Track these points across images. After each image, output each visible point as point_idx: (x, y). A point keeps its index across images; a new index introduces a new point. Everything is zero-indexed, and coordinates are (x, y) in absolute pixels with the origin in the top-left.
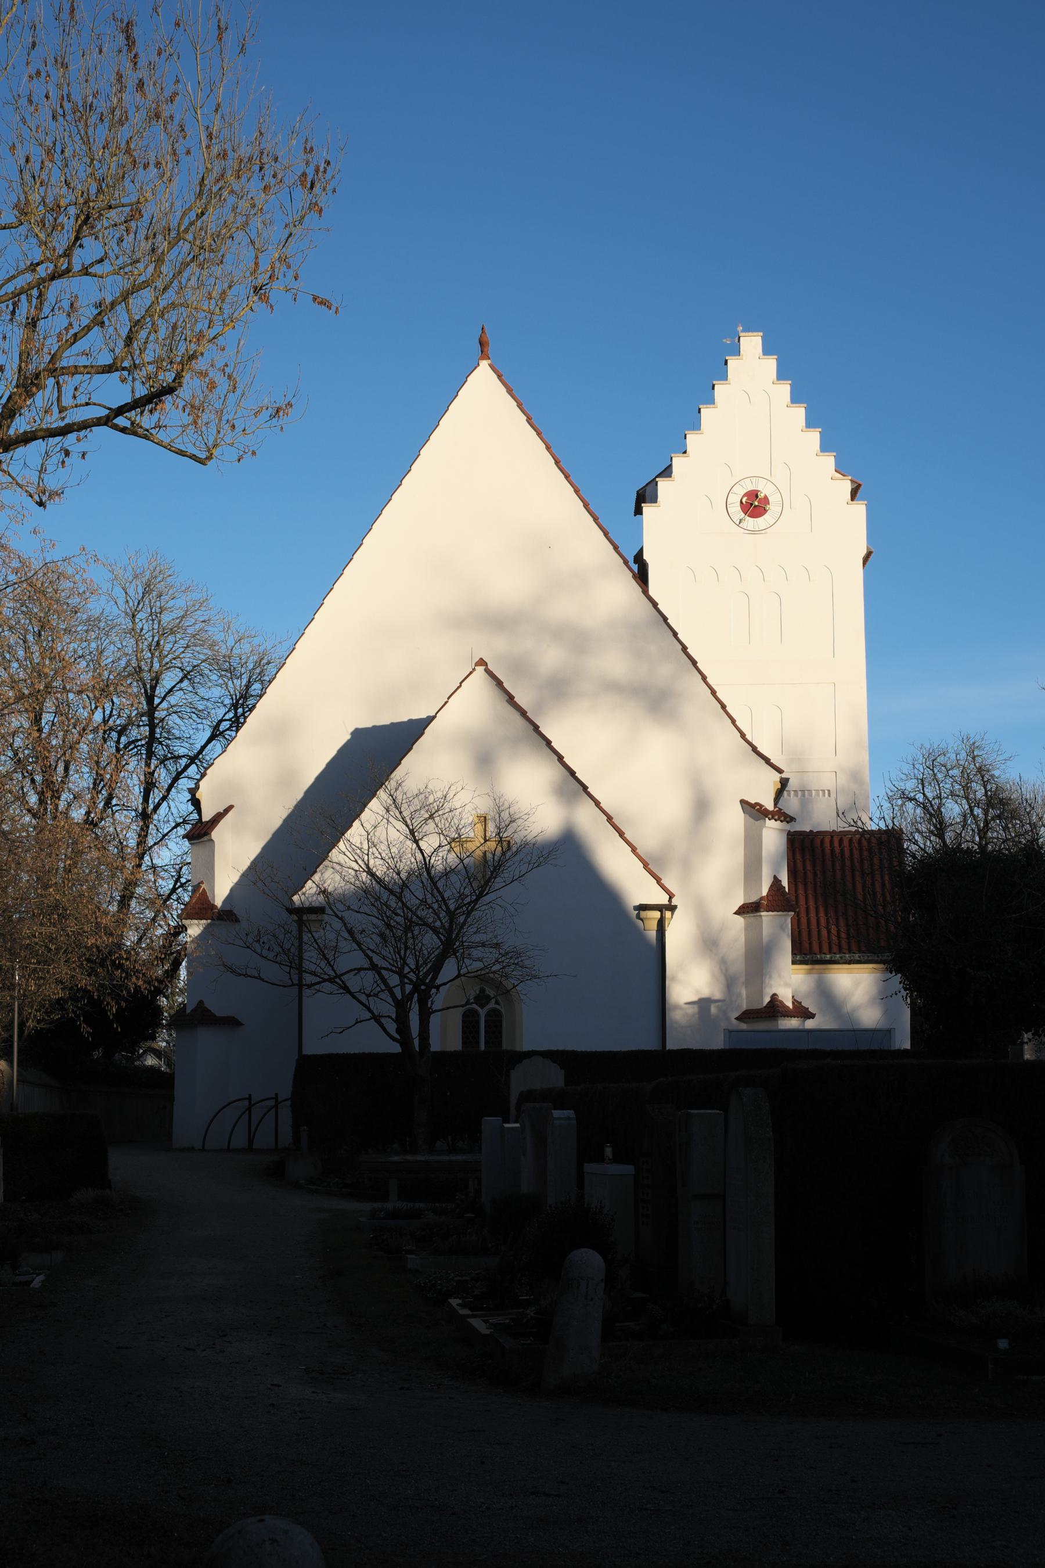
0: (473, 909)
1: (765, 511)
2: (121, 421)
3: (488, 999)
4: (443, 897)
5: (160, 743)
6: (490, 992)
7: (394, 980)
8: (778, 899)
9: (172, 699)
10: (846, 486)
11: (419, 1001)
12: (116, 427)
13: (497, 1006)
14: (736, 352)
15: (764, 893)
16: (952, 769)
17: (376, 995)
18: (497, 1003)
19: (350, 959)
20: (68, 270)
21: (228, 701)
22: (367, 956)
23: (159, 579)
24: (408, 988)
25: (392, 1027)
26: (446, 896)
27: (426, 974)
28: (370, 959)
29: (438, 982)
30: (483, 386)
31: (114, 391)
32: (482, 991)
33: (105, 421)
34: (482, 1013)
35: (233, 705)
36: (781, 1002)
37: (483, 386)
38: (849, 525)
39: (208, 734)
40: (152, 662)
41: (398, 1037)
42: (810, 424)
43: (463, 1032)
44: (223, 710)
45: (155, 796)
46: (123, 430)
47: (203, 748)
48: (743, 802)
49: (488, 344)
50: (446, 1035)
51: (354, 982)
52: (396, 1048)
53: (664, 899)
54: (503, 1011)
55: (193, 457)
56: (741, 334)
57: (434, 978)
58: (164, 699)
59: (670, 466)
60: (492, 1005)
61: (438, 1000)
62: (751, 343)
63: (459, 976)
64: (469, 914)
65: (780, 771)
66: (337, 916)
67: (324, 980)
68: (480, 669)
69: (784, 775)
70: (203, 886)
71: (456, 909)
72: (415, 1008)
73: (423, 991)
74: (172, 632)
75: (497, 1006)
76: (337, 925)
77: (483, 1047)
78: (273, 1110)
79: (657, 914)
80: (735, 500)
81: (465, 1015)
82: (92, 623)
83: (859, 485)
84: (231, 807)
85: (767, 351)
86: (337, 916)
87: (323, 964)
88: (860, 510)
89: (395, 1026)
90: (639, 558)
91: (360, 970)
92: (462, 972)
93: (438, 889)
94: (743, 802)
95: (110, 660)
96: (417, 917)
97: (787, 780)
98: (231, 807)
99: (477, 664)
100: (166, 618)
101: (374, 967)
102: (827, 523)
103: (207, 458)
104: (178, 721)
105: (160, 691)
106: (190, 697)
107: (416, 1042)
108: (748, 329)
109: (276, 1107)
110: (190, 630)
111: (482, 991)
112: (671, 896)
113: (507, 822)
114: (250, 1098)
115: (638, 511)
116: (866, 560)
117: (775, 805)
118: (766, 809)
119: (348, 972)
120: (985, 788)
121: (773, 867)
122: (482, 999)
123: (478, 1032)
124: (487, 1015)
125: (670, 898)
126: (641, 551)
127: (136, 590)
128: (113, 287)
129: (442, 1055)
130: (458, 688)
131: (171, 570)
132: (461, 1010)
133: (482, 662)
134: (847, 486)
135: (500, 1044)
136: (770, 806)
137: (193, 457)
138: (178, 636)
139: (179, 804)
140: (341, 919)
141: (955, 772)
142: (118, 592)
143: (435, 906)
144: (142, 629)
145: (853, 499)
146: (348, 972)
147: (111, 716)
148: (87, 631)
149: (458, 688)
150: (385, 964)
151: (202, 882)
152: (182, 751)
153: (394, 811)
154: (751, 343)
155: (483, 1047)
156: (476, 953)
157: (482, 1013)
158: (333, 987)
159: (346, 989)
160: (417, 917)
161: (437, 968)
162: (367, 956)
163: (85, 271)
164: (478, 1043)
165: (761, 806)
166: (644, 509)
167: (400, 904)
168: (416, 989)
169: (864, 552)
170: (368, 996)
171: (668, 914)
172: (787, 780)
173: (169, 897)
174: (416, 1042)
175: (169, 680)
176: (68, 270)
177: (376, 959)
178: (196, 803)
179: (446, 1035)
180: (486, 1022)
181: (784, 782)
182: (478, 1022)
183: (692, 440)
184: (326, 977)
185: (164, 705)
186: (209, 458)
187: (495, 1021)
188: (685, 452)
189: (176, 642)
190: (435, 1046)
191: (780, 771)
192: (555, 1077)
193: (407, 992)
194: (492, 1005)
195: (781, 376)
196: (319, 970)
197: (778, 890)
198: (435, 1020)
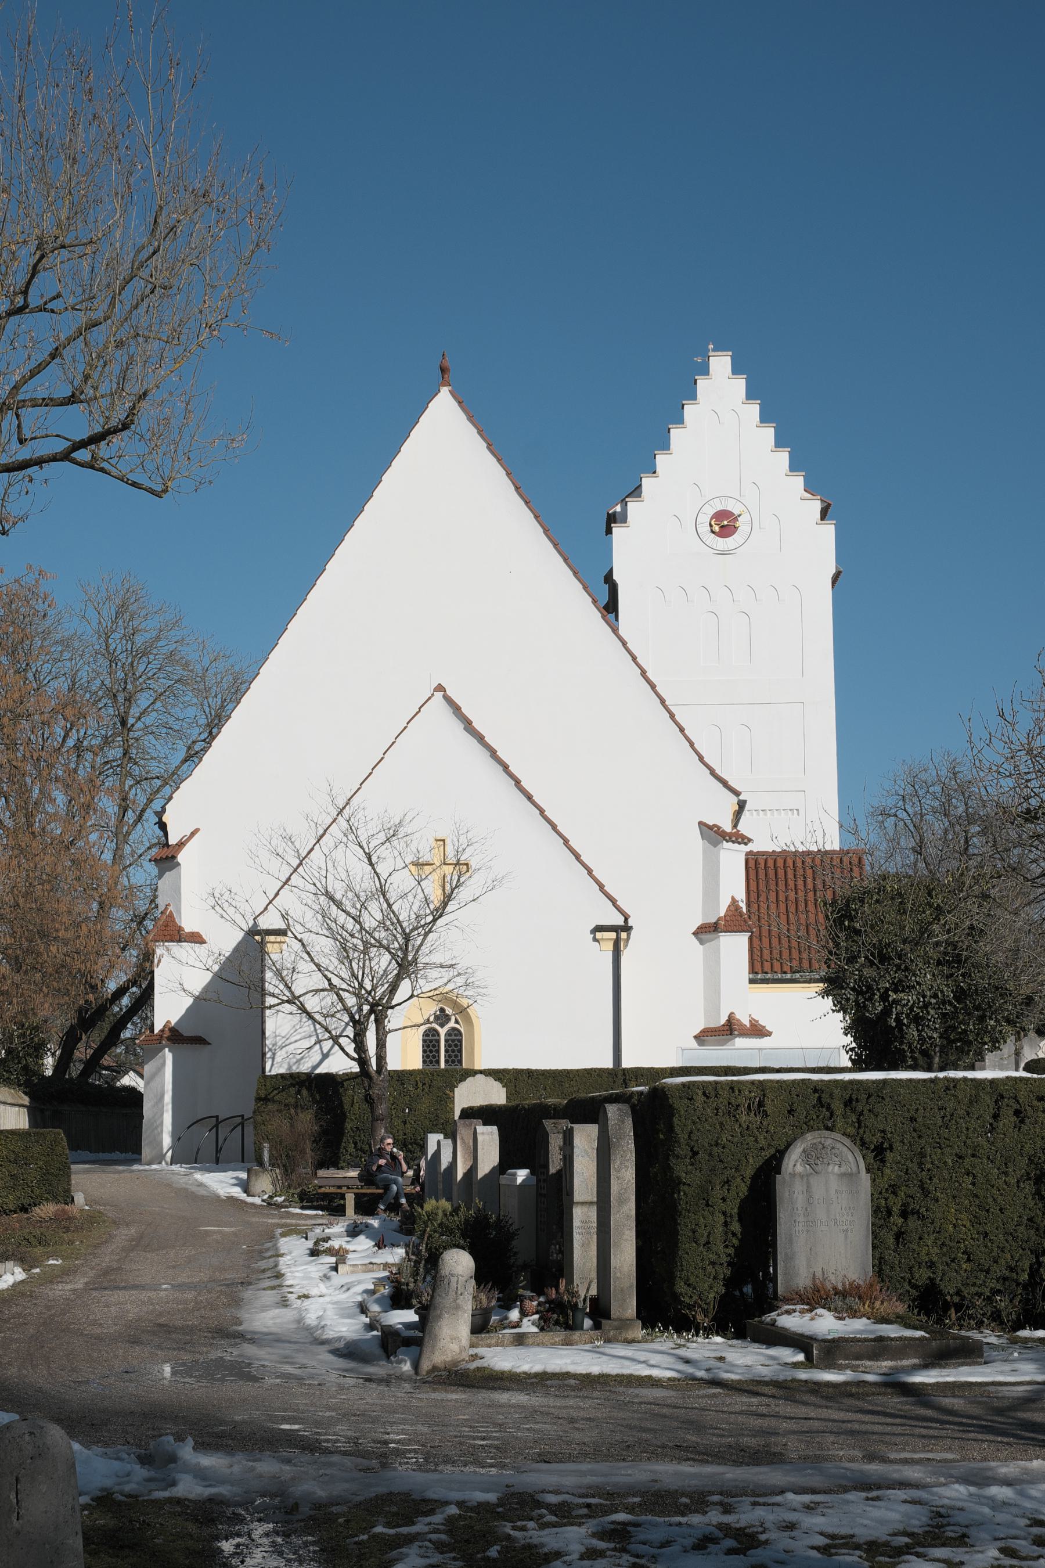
0: (430, 931)
1: (736, 528)
2: (83, 455)
3: (448, 1019)
4: (398, 920)
5: (136, 763)
6: (449, 1011)
7: (351, 1001)
8: (732, 921)
9: (148, 720)
10: (815, 506)
11: (376, 1021)
12: (74, 462)
13: (457, 1026)
14: (705, 371)
15: (722, 914)
16: (933, 785)
17: (332, 1016)
18: (457, 1022)
19: (306, 980)
20: (25, 306)
21: (203, 721)
22: (325, 976)
23: (132, 600)
24: (366, 1008)
25: (350, 1048)
26: (401, 918)
27: (383, 995)
28: (329, 980)
29: (394, 1003)
30: (443, 411)
31: (77, 423)
32: (442, 1010)
33: (65, 456)
34: (443, 1032)
35: (208, 725)
36: (738, 1020)
37: (443, 411)
38: (816, 546)
39: (182, 754)
40: (126, 683)
41: (356, 1056)
42: (779, 443)
43: (424, 1051)
44: (197, 731)
45: (130, 816)
46: (81, 465)
47: (178, 768)
48: (700, 823)
49: (448, 370)
50: (405, 1054)
51: (312, 1003)
52: (356, 1069)
53: (620, 921)
54: (462, 1030)
55: (152, 492)
56: (711, 353)
57: (391, 999)
58: (139, 718)
59: (640, 485)
60: (452, 1024)
61: (394, 1019)
62: (721, 363)
63: (412, 996)
64: (426, 934)
65: (737, 793)
66: (296, 938)
67: (283, 1002)
68: (439, 695)
69: (741, 798)
70: (170, 908)
71: (412, 931)
72: (372, 1027)
73: (379, 1010)
74: (145, 654)
75: (457, 1026)
76: (297, 946)
77: (443, 1065)
78: (240, 1127)
79: (613, 935)
80: (705, 519)
81: (426, 1034)
82: (66, 643)
83: (829, 505)
84: (197, 831)
85: (736, 370)
86: (296, 938)
87: (282, 987)
88: (829, 530)
89: (353, 1045)
90: (609, 579)
91: (317, 991)
92: (415, 993)
93: (393, 912)
94: (700, 823)
95: (84, 680)
96: (375, 939)
97: (745, 802)
98: (197, 831)
99: (435, 690)
100: (139, 640)
101: (332, 987)
102: (796, 542)
103: (163, 491)
104: (154, 741)
105: (135, 711)
106: (165, 718)
107: (374, 1062)
108: (719, 348)
109: (242, 1124)
110: (164, 650)
111: (442, 1010)
112: (626, 920)
113: (464, 846)
114: (242, 1116)
115: (609, 531)
116: (835, 579)
117: (735, 826)
118: (723, 831)
119: (306, 993)
120: (966, 805)
121: (733, 886)
122: (442, 1018)
123: (438, 1051)
124: (448, 1034)
125: (626, 920)
126: (611, 571)
127: (109, 610)
128: (69, 323)
129: (401, 1076)
130: (417, 713)
131: (144, 591)
132: (423, 1028)
133: (440, 688)
134: (816, 506)
135: (460, 1062)
136: (728, 828)
137: (152, 492)
138: (152, 657)
139: (148, 829)
140: (300, 941)
141: (937, 789)
142: (91, 613)
143: (391, 927)
144: (114, 651)
145: (822, 519)
146: (306, 993)
147: (84, 738)
148: (61, 652)
149: (417, 713)
150: (344, 986)
151: (169, 905)
152: (156, 772)
153: (351, 837)
154: (721, 363)
155: (443, 1065)
156: (433, 973)
157: (443, 1032)
158: (292, 1008)
159: (303, 1009)
160: (375, 939)
161: (393, 988)
162: (325, 976)
163: (41, 309)
164: (438, 1062)
165: (719, 828)
166: (614, 529)
167: (358, 927)
168: (372, 1011)
169: (833, 571)
170: (325, 1016)
171: (624, 935)
172: (745, 802)
173: (144, 919)
174: (374, 1062)
175: (143, 700)
176: (25, 306)
177: (335, 981)
178: (163, 826)
179: (405, 1054)
180: (446, 1041)
181: (742, 805)
182: (438, 1041)
183: (662, 460)
184: (286, 998)
185: (139, 725)
186: (165, 491)
187: (455, 1042)
188: (655, 472)
189: (149, 663)
190: (394, 1063)
191: (737, 793)
192: (497, 1095)
193: (365, 1012)
194: (452, 1024)
195: (750, 395)
196: (277, 991)
197: (736, 910)
198: (390, 1039)
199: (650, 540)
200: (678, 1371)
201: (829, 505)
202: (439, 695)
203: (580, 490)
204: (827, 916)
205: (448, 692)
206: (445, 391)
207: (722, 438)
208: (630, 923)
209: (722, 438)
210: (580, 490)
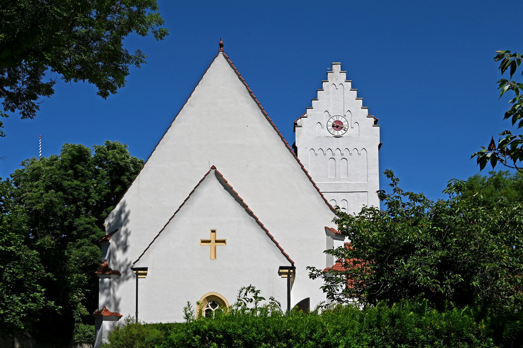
38: (374, 135)
48: (326, 228)
62: (337, 68)
84: (203, 242)
94: (326, 228)
98: (203, 242)
102: (365, 133)
116: (380, 146)
133: (213, 168)
134: (372, 120)
199: (311, 129)
200: (509, 65)
201: (377, 120)
202: (213, 171)
203: (284, 107)
204: (114, 147)
205: (218, 169)
206: (221, 55)
207: (337, 95)
208: (295, 265)
209: (337, 95)
210: (284, 107)
